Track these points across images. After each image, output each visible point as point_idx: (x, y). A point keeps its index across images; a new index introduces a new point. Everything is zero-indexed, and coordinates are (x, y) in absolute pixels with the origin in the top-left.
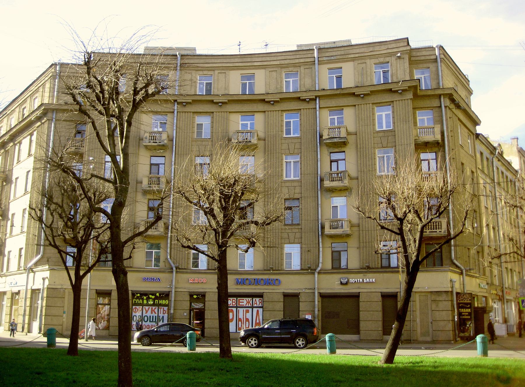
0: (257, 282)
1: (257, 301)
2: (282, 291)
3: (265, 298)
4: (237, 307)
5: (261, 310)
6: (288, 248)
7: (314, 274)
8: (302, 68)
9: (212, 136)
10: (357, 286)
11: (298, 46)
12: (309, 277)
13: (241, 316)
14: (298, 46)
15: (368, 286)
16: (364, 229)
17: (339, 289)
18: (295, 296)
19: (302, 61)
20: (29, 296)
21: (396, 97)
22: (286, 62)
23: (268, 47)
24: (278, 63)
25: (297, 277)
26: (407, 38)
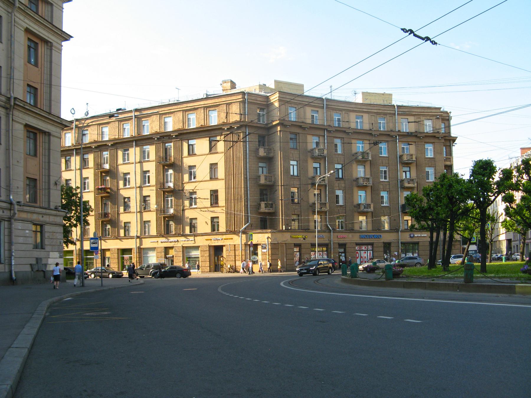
0: (370, 237)
1: (370, 247)
2: (382, 241)
3: (375, 245)
4: (360, 251)
5: (371, 252)
6: (383, 218)
7: (398, 232)
8: (388, 116)
9: (344, 152)
10: (417, 238)
11: (365, 94)
12: (395, 234)
13: (362, 255)
14: (365, 94)
15: (422, 238)
16: (41, 188)
17: (408, 240)
18: (389, 244)
19: (388, 112)
20: (244, 248)
21: (436, 141)
22: (380, 111)
23: (353, 92)
24: (376, 111)
25: (387, 234)
26: (522, 149)
